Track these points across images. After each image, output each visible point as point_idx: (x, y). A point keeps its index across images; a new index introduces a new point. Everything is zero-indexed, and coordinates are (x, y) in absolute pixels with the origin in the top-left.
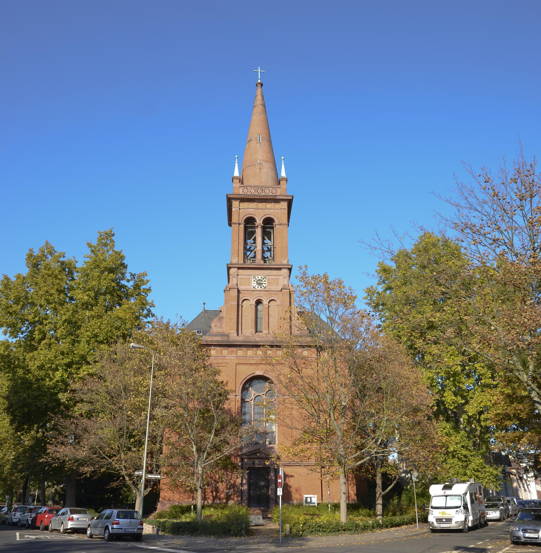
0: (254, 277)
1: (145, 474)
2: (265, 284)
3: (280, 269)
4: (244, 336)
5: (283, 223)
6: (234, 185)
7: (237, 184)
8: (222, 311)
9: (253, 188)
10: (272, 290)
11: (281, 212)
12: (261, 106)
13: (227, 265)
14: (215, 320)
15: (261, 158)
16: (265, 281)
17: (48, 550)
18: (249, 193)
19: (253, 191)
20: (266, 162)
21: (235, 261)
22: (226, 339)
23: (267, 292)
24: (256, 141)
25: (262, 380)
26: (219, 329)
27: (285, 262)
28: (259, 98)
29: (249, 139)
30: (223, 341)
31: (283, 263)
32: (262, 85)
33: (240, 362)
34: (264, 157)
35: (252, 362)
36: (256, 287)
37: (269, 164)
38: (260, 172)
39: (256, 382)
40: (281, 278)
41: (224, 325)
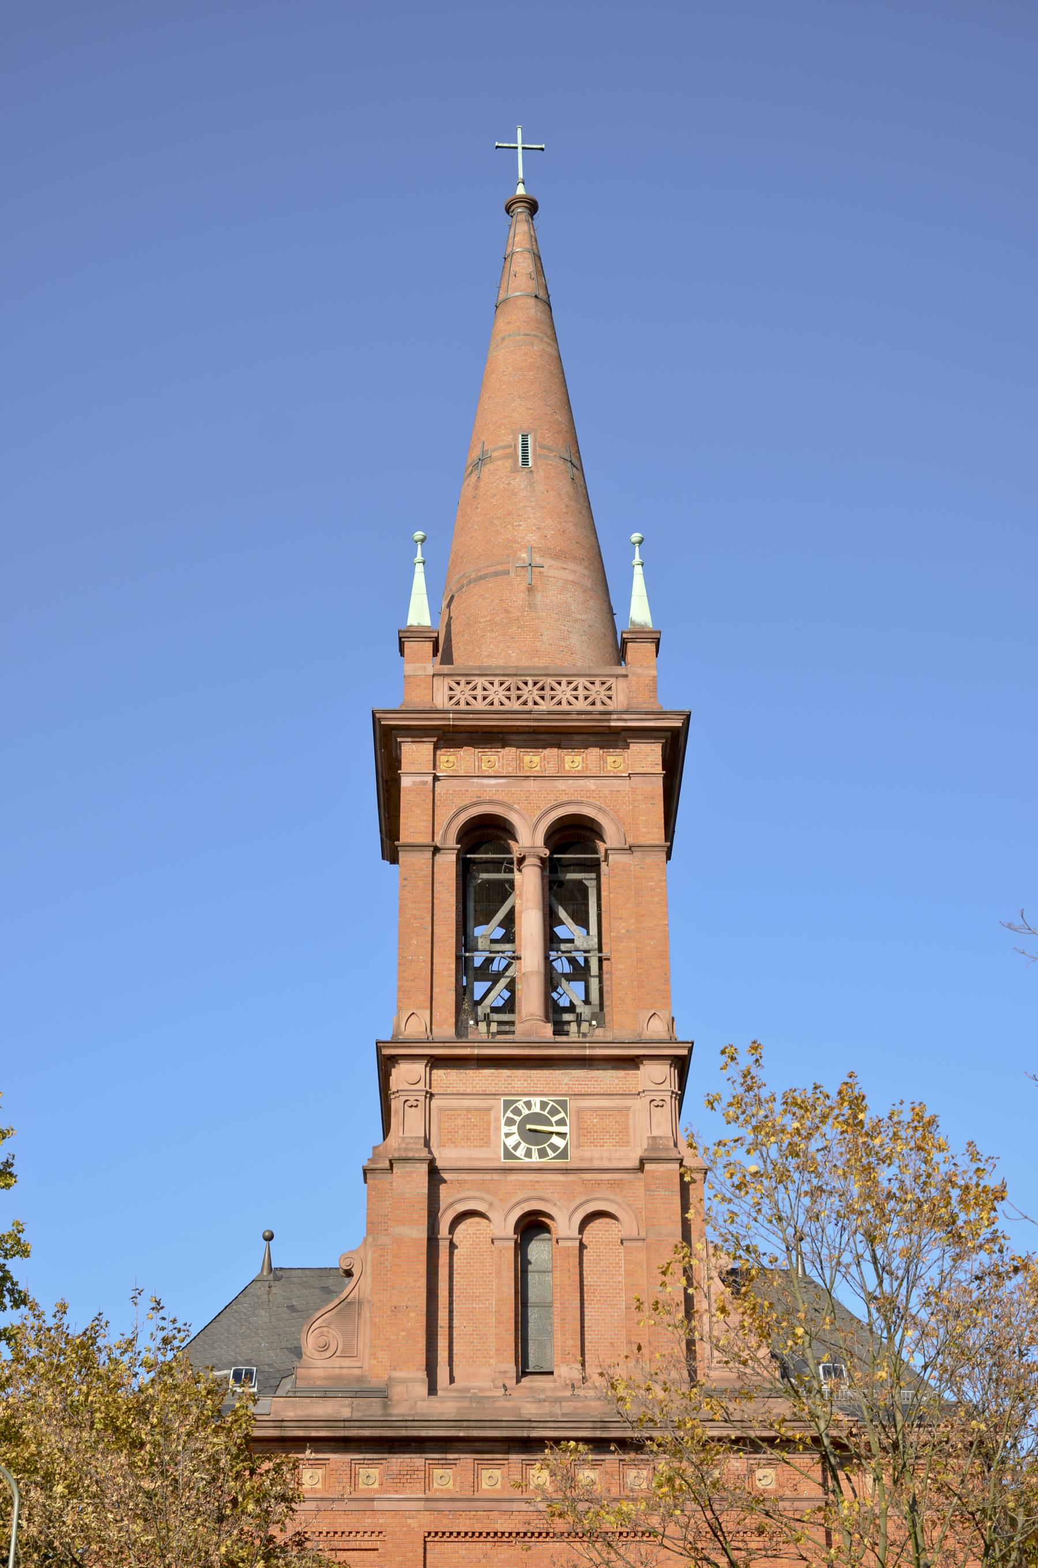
0: (508, 1104)
3: (632, 1062)
5: (642, 841)
6: (409, 668)
8: (356, 1272)
10: (597, 1164)
11: (633, 790)
12: (532, 302)
13: (379, 1046)
15: (532, 538)
16: (561, 1122)
18: (480, 705)
20: (556, 556)
21: (415, 1028)
22: (373, 1409)
23: (571, 1177)
24: (508, 463)
27: (657, 1028)
28: (522, 264)
29: (476, 453)
32: (533, 207)
34: (550, 533)
35: (503, 1525)
36: (520, 1152)
37: (571, 566)
38: (531, 606)
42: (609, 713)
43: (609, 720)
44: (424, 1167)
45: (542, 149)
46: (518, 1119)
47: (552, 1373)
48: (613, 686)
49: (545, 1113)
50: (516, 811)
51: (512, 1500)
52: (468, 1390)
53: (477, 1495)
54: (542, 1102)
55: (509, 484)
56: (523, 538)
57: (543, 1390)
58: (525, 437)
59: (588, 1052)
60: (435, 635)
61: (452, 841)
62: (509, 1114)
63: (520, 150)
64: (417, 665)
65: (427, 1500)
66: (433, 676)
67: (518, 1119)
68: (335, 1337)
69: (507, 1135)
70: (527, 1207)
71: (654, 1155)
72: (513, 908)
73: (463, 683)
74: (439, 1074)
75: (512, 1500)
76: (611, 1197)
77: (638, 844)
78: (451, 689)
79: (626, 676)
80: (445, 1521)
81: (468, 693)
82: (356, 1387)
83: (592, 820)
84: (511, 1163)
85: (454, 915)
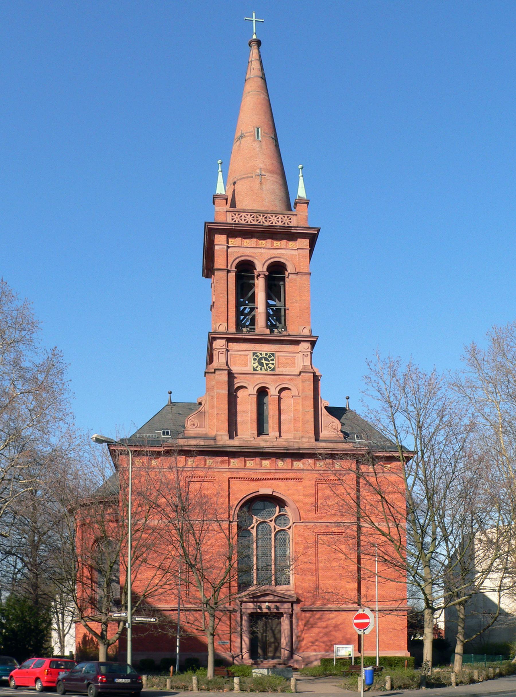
0: (254, 354)
1: (132, 615)
2: (273, 364)
3: (297, 343)
4: (240, 439)
5: (302, 271)
6: (217, 209)
7: (221, 207)
8: (203, 403)
9: (249, 214)
10: (284, 373)
11: (299, 254)
12: (260, 79)
13: (210, 333)
14: (192, 416)
15: (261, 165)
16: (272, 360)
17: (255, 578)
18: (243, 222)
19: (250, 219)
20: (270, 172)
21: (222, 328)
22: (211, 442)
23: (275, 377)
24: (252, 138)
25: (270, 502)
26: (198, 429)
27: (306, 332)
28: (255, 65)
29: (238, 134)
30: (208, 446)
31: (302, 334)
32: (259, 43)
33: (235, 475)
34: (268, 164)
35: (254, 476)
36: (258, 369)
37: (275, 176)
38: (261, 189)
39: (259, 505)
40: (300, 355)
41: (207, 422)
42: (291, 227)
43: (291, 230)
44: (226, 372)
45: (263, 22)
46: (258, 358)
47: (268, 434)
48: (292, 218)
49: (267, 357)
50: (256, 259)
51: (257, 469)
52: (242, 438)
53: (245, 468)
54: (266, 354)
55: (252, 145)
56: (258, 165)
57: (266, 439)
58: (258, 130)
59: (282, 338)
60: (227, 197)
61: (233, 269)
62: (254, 357)
63: (254, 21)
64: (220, 208)
65: (229, 468)
66: (226, 211)
67: (258, 358)
68: (196, 422)
69: (254, 363)
70: (258, 387)
71: (304, 371)
72: (254, 292)
73: (237, 215)
74: (230, 344)
75: (257, 469)
76: (289, 383)
77: (300, 272)
78: (232, 216)
79: (296, 215)
80: (235, 474)
81: (239, 218)
82: (204, 436)
83: (284, 264)
84: (255, 372)
85: (235, 293)
